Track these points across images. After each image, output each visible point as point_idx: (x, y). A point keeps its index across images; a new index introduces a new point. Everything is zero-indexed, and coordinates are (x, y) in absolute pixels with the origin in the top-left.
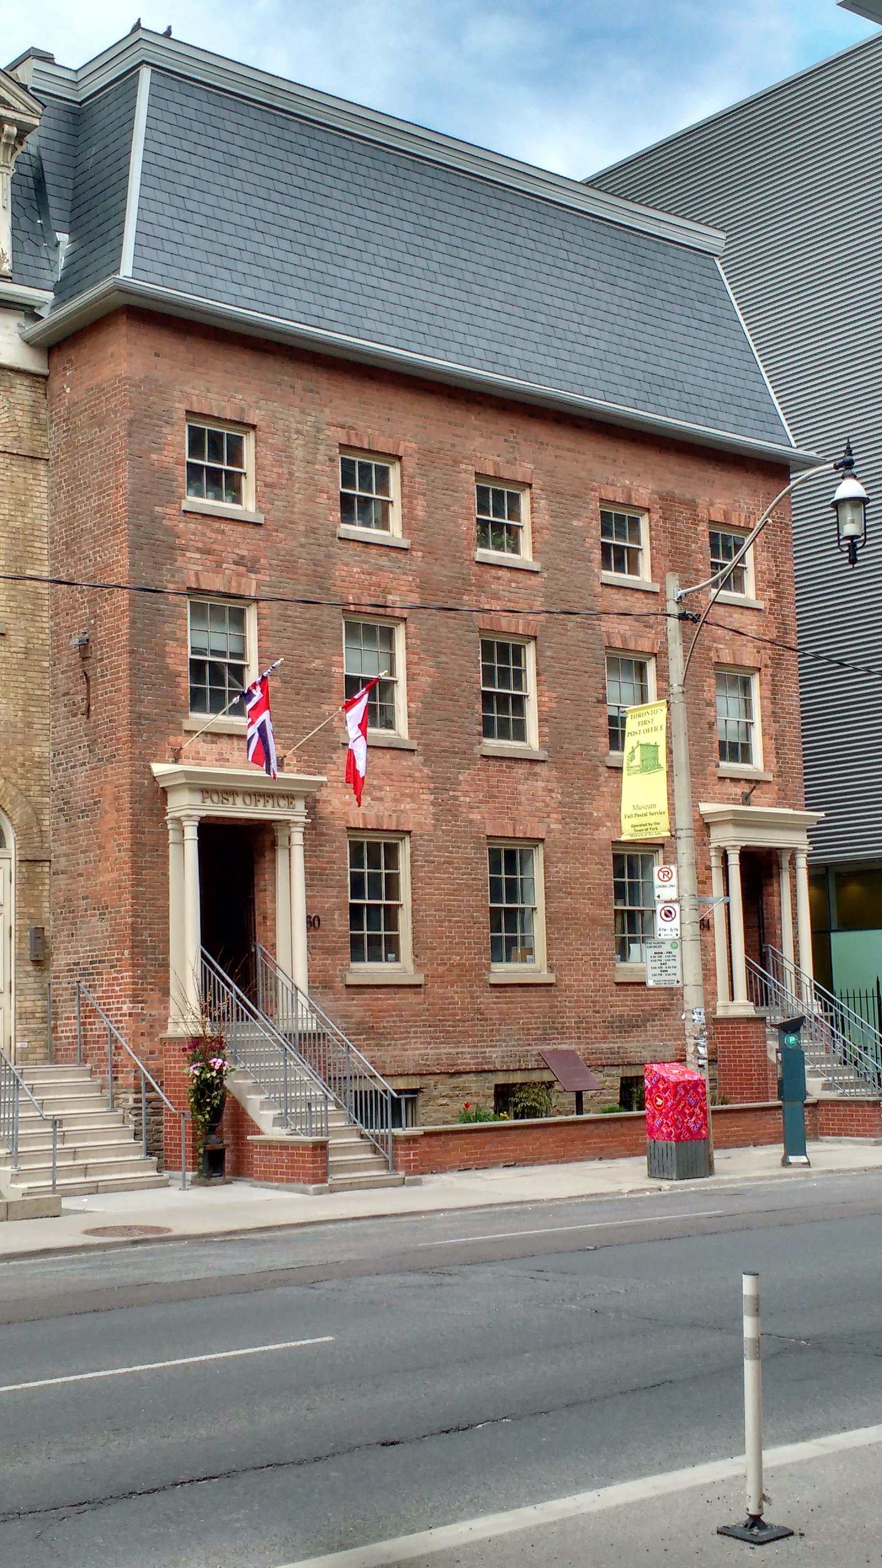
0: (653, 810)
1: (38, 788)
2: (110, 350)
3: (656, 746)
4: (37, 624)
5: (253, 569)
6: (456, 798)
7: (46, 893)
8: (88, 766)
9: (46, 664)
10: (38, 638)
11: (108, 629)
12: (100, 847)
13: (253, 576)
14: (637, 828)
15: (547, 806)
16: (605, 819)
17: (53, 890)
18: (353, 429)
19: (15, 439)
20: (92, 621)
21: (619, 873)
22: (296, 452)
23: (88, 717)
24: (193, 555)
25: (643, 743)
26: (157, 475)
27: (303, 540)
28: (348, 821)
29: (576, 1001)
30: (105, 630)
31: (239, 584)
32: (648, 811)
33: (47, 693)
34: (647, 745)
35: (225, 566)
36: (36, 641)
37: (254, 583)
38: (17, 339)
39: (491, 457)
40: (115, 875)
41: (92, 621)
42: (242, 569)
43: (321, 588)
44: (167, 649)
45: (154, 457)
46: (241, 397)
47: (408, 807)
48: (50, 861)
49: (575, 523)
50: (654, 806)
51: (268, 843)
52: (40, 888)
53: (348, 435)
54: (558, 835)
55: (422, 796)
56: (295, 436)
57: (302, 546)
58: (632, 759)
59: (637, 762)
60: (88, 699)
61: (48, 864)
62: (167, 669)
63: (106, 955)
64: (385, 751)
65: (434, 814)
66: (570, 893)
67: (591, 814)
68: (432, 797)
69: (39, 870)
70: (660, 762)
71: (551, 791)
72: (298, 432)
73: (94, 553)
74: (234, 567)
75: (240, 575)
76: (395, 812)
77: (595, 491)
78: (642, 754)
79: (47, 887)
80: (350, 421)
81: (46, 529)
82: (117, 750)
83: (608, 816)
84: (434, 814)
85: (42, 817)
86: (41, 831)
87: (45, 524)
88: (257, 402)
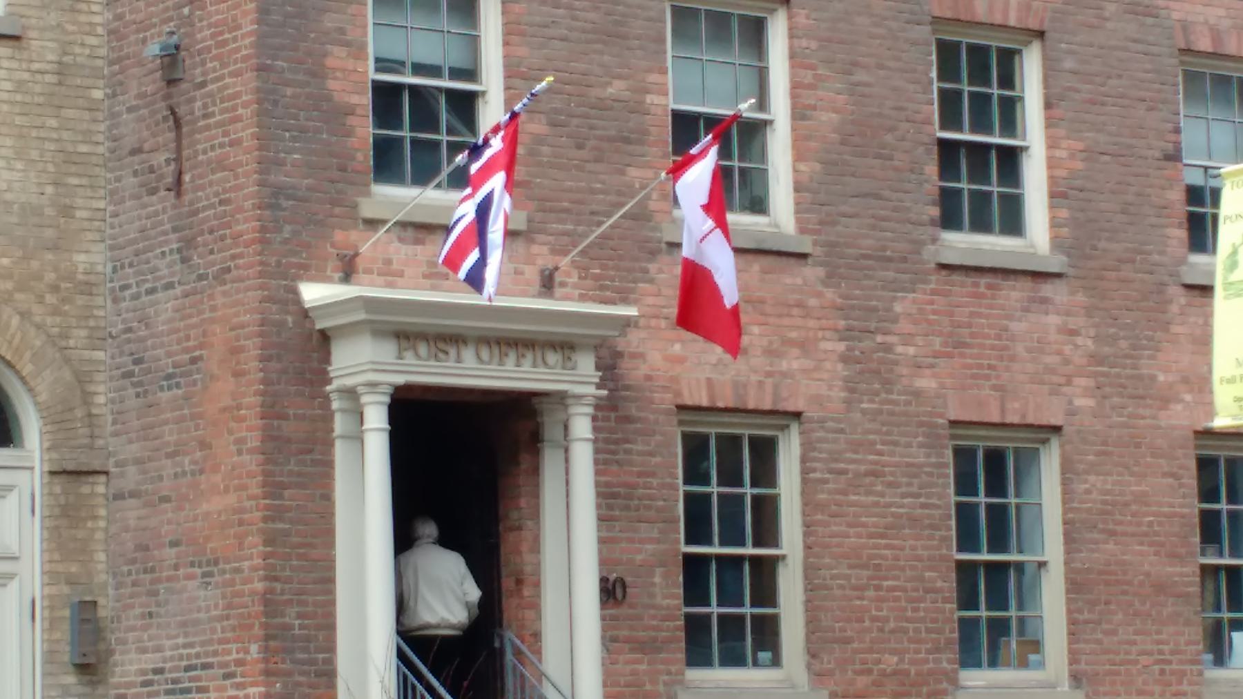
6: (888, 348)
7: (99, 535)
10: (83, 45)
15: (1067, 362)
20: (186, 11)
28: (678, 394)
30: (210, 26)
44: (330, 62)
60: (178, 160)
61: (103, 478)
66: (1113, 533)
68: (841, 347)
69: (86, 489)
71: (1073, 333)
76: (769, 374)
79: (102, 524)
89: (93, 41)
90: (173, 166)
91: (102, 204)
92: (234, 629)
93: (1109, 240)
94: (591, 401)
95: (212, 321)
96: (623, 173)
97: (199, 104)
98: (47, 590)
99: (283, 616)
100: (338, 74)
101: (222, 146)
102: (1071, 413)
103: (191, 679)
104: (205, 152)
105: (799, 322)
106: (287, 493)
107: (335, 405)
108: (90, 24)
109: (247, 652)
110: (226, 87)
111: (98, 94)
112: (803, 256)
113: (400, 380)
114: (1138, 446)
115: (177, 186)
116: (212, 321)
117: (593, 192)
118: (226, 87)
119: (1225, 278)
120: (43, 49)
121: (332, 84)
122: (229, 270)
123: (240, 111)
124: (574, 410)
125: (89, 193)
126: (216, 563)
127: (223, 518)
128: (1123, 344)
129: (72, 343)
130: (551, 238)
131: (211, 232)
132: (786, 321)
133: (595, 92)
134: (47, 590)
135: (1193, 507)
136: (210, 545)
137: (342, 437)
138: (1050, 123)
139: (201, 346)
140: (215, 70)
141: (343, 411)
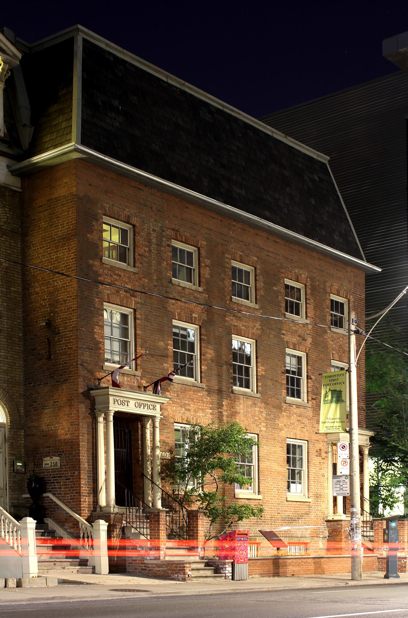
1: (18, 394)
4: (16, 315)
7: (23, 445)
11: (63, 318)
13: (133, 299)
15: (260, 419)
16: (284, 427)
18: (179, 232)
20: (52, 315)
21: (288, 452)
22: (153, 240)
27: (155, 283)
29: (270, 508)
30: (60, 319)
34: (335, 391)
35: (121, 292)
37: (134, 302)
38: (6, 170)
39: (239, 252)
41: (52, 315)
42: (128, 295)
43: (163, 307)
45: (89, 235)
47: (201, 414)
49: (274, 288)
53: (176, 234)
54: (264, 432)
55: (207, 410)
56: (152, 232)
57: (155, 286)
60: (49, 352)
63: (63, 474)
66: (269, 460)
67: (278, 424)
68: (211, 411)
71: (262, 412)
72: (154, 230)
73: (53, 281)
74: (125, 293)
75: (128, 298)
76: (195, 416)
77: (283, 273)
79: (23, 442)
80: (177, 227)
82: (69, 377)
83: (285, 425)
84: (212, 419)
88: (135, 213)
89: (19, 321)
90: (47, 354)
93: (270, 391)
96: (162, 364)
98: (10, 458)
101: (65, 349)
102: (260, 431)
103: (54, 480)
104: (59, 350)
109: (74, 473)
110: (67, 334)
111: (21, 335)
114: (275, 440)
115: (49, 358)
117: (156, 368)
118: (67, 334)
121: (96, 336)
126: (63, 452)
128: (272, 416)
129: (15, 397)
132: (199, 404)
134: (10, 458)
135: (285, 456)
140: (62, 330)
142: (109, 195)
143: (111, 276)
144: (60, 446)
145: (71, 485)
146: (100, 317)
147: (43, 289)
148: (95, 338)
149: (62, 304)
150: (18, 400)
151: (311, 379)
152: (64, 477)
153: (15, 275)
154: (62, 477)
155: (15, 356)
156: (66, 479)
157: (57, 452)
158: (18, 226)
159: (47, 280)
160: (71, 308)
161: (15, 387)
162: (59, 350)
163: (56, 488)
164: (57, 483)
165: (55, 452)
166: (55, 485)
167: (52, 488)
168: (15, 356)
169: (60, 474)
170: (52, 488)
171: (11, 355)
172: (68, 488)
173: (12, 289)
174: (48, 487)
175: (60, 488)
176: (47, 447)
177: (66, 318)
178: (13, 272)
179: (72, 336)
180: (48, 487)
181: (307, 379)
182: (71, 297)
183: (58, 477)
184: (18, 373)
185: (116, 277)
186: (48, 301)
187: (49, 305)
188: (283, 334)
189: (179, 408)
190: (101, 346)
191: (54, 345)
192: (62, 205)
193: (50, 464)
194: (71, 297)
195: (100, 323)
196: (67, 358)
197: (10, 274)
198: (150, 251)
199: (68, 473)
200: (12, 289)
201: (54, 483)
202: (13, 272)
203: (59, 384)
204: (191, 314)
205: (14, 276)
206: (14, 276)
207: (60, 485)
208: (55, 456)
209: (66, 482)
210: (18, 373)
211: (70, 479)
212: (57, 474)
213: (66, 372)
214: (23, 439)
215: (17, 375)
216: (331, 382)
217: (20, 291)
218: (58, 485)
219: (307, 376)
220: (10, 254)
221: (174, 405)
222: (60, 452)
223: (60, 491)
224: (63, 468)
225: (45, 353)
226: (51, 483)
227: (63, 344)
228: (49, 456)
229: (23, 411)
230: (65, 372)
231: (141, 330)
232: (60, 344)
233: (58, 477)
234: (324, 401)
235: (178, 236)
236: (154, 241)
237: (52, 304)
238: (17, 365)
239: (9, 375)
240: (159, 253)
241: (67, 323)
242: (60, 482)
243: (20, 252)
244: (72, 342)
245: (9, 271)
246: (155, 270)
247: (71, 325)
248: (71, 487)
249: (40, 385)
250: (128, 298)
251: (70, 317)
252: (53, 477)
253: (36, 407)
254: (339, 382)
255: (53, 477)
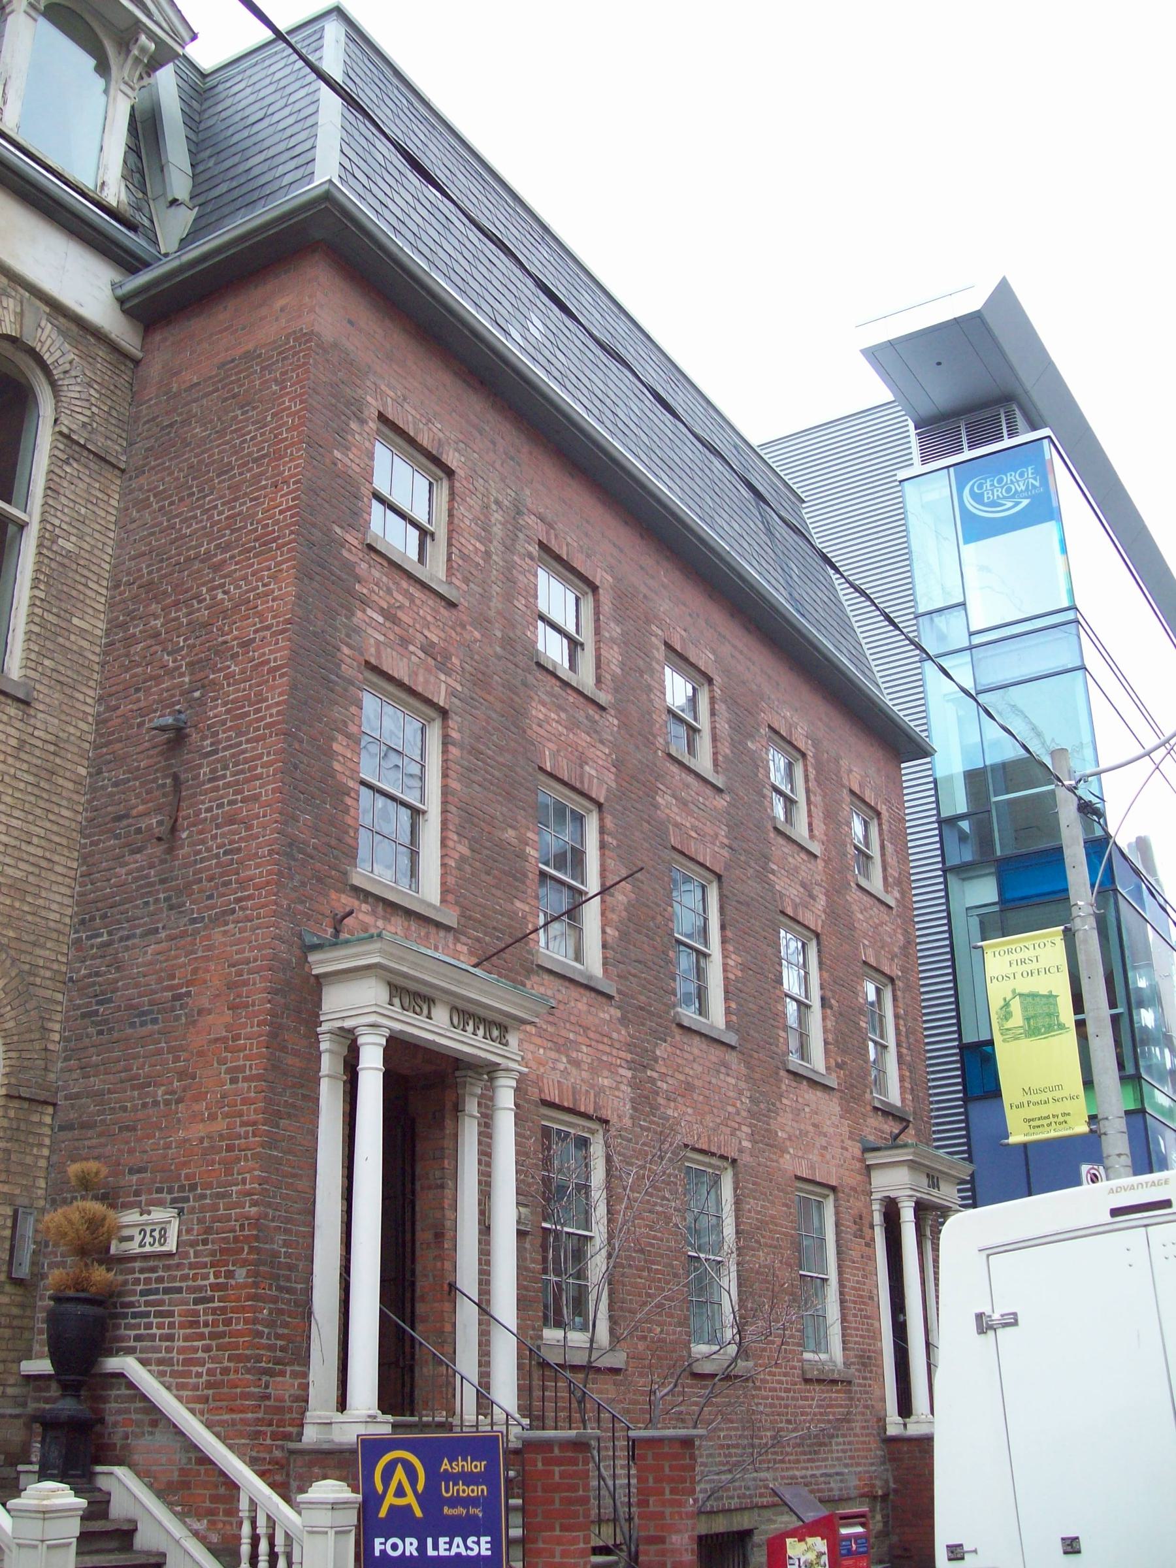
0: (1058, 1094)
2: (279, 303)
3: (1051, 997)
5: (443, 665)
6: (652, 1080)
7: (43, 1163)
8: (163, 935)
9: (83, 772)
10: (76, 727)
12: (182, 1075)
14: (1032, 1123)
16: (788, 1143)
17: (54, 1158)
19: (84, 425)
23: (171, 850)
24: (375, 615)
25: (1025, 991)
26: (340, 481)
28: (541, 1091)
30: (225, 704)
31: (427, 682)
32: (1050, 1095)
33: (79, 818)
36: (72, 730)
40: (221, 1125)
41: (197, 694)
44: (335, 746)
45: (337, 454)
46: (439, 426)
48: (54, 1105)
50: (1059, 1087)
51: (449, 1105)
52: (35, 1151)
56: (494, 507)
58: (1007, 1016)
59: (1017, 1020)
61: (50, 1110)
62: (334, 777)
63: (184, 1278)
64: (582, 991)
65: (632, 1100)
69: (35, 1118)
70: (1062, 1019)
72: (497, 502)
73: (210, 590)
78: (1025, 1009)
79: (46, 1152)
80: (549, 517)
81: (107, 567)
85: (50, 1025)
86: (46, 1049)
87: (108, 558)
89: (84, 726)
91: (75, 865)
92: (213, 1253)
94: (516, 1075)
95: (206, 959)
97: (206, 769)
99: (272, 1242)
100: (340, 758)
101: (231, 803)
103: (147, 1303)
105: (607, 1049)
106: (283, 1122)
107: (324, 1046)
108: (84, 712)
109: (230, 1275)
110: (244, 752)
111: (83, 771)
112: (610, 997)
113: (398, 1026)
116: (206, 959)
118: (244, 752)
119: (1001, 1025)
120: (44, 722)
122: (233, 911)
123: (259, 770)
124: (502, 1082)
125: (66, 852)
126: (193, 1187)
127: (206, 1144)
128: (762, 1106)
130: (470, 941)
131: (211, 879)
132: (601, 1047)
133: (498, 833)
136: (183, 1173)
137: (328, 1076)
138: (724, 941)
139: (189, 983)
141: (330, 1051)
142: (395, 367)
143: (389, 591)
144: (185, 1164)
145: (215, 1323)
146: (353, 709)
147: (177, 618)
148: (332, 773)
149: (236, 655)
150: (48, 994)
151: (831, 1007)
152: (191, 1290)
153: (91, 584)
154: (179, 1290)
155: (57, 839)
156: (197, 1302)
157: (170, 1191)
158: (117, 448)
159: (191, 588)
160: (268, 662)
161: (43, 947)
162: (209, 810)
163: (152, 1337)
164: (159, 1314)
165: (160, 1190)
166: (149, 1326)
167: (138, 1338)
168: (57, 839)
169: (173, 1279)
170: (138, 1338)
171: (42, 832)
172: (201, 1337)
173: (75, 621)
174: (122, 1332)
175: (170, 1338)
176: (132, 1171)
177: (247, 698)
178: (85, 572)
179: (260, 757)
180: (122, 1332)
181: (823, 1006)
182: (268, 628)
183: (167, 1291)
184: (58, 898)
185: (400, 598)
186: (188, 655)
187: (190, 664)
188: (773, 872)
189: (553, 1055)
190: (349, 801)
191: (194, 795)
192: (263, 369)
193: (138, 1238)
194: (268, 628)
195: (352, 729)
196: (234, 833)
197: (78, 578)
198: (488, 554)
199: (205, 1277)
200: (75, 621)
201: (147, 1315)
202: (85, 572)
203: (196, 932)
204: (582, 767)
205: (86, 585)
206: (86, 585)
207: (171, 1325)
208: (160, 1203)
209: (196, 1313)
210: (58, 898)
211: (211, 1300)
212: (160, 1280)
213: (226, 884)
214: (47, 1141)
215: (54, 907)
216: (1014, 968)
217: (99, 633)
218: (160, 1326)
219: (823, 999)
220: (85, 517)
221: (538, 1041)
222: (182, 1188)
223: (169, 1350)
224: (186, 1255)
225: (160, 823)
226: (135, 1315)
227: (228, 785)
228: (138, 1204)
229: (56, 1037)
230: (226, 884)
231: (459, 781)
232: (217, 789)
233: (167, 1291)
234: (1004, 1032)
235: (553, 536)
236: (497, 530)
237: (200, 661)
238: (58, 869)
239: (29, 899)
240: (509, 570)
241: (247, 714)
242: (170, 1314)
243: (113, 519)
244: (259, 777)
245: (74, 566)
246: (499, 613)
247: (263, 718)
248: (213, 1336)
249: (128, 938)
250: (428, 670)
251: (260, 693)
252: (143, 1293)
253: (106, 1022)
254: (1041, 965)
255: (143, 1293)
